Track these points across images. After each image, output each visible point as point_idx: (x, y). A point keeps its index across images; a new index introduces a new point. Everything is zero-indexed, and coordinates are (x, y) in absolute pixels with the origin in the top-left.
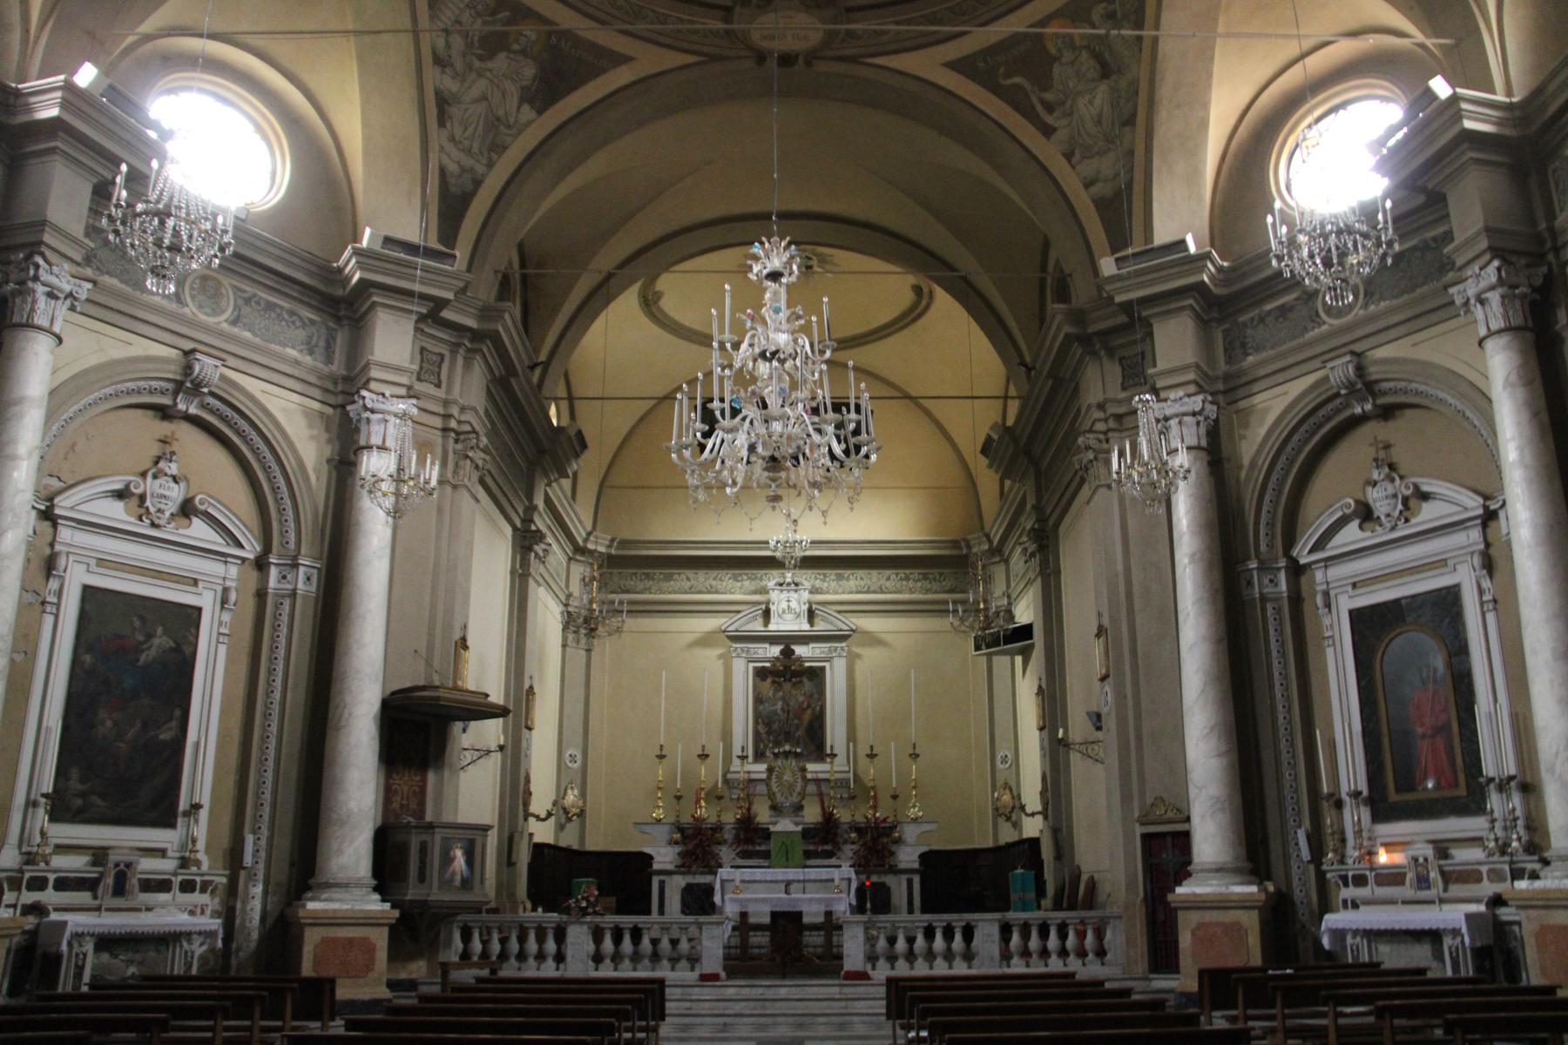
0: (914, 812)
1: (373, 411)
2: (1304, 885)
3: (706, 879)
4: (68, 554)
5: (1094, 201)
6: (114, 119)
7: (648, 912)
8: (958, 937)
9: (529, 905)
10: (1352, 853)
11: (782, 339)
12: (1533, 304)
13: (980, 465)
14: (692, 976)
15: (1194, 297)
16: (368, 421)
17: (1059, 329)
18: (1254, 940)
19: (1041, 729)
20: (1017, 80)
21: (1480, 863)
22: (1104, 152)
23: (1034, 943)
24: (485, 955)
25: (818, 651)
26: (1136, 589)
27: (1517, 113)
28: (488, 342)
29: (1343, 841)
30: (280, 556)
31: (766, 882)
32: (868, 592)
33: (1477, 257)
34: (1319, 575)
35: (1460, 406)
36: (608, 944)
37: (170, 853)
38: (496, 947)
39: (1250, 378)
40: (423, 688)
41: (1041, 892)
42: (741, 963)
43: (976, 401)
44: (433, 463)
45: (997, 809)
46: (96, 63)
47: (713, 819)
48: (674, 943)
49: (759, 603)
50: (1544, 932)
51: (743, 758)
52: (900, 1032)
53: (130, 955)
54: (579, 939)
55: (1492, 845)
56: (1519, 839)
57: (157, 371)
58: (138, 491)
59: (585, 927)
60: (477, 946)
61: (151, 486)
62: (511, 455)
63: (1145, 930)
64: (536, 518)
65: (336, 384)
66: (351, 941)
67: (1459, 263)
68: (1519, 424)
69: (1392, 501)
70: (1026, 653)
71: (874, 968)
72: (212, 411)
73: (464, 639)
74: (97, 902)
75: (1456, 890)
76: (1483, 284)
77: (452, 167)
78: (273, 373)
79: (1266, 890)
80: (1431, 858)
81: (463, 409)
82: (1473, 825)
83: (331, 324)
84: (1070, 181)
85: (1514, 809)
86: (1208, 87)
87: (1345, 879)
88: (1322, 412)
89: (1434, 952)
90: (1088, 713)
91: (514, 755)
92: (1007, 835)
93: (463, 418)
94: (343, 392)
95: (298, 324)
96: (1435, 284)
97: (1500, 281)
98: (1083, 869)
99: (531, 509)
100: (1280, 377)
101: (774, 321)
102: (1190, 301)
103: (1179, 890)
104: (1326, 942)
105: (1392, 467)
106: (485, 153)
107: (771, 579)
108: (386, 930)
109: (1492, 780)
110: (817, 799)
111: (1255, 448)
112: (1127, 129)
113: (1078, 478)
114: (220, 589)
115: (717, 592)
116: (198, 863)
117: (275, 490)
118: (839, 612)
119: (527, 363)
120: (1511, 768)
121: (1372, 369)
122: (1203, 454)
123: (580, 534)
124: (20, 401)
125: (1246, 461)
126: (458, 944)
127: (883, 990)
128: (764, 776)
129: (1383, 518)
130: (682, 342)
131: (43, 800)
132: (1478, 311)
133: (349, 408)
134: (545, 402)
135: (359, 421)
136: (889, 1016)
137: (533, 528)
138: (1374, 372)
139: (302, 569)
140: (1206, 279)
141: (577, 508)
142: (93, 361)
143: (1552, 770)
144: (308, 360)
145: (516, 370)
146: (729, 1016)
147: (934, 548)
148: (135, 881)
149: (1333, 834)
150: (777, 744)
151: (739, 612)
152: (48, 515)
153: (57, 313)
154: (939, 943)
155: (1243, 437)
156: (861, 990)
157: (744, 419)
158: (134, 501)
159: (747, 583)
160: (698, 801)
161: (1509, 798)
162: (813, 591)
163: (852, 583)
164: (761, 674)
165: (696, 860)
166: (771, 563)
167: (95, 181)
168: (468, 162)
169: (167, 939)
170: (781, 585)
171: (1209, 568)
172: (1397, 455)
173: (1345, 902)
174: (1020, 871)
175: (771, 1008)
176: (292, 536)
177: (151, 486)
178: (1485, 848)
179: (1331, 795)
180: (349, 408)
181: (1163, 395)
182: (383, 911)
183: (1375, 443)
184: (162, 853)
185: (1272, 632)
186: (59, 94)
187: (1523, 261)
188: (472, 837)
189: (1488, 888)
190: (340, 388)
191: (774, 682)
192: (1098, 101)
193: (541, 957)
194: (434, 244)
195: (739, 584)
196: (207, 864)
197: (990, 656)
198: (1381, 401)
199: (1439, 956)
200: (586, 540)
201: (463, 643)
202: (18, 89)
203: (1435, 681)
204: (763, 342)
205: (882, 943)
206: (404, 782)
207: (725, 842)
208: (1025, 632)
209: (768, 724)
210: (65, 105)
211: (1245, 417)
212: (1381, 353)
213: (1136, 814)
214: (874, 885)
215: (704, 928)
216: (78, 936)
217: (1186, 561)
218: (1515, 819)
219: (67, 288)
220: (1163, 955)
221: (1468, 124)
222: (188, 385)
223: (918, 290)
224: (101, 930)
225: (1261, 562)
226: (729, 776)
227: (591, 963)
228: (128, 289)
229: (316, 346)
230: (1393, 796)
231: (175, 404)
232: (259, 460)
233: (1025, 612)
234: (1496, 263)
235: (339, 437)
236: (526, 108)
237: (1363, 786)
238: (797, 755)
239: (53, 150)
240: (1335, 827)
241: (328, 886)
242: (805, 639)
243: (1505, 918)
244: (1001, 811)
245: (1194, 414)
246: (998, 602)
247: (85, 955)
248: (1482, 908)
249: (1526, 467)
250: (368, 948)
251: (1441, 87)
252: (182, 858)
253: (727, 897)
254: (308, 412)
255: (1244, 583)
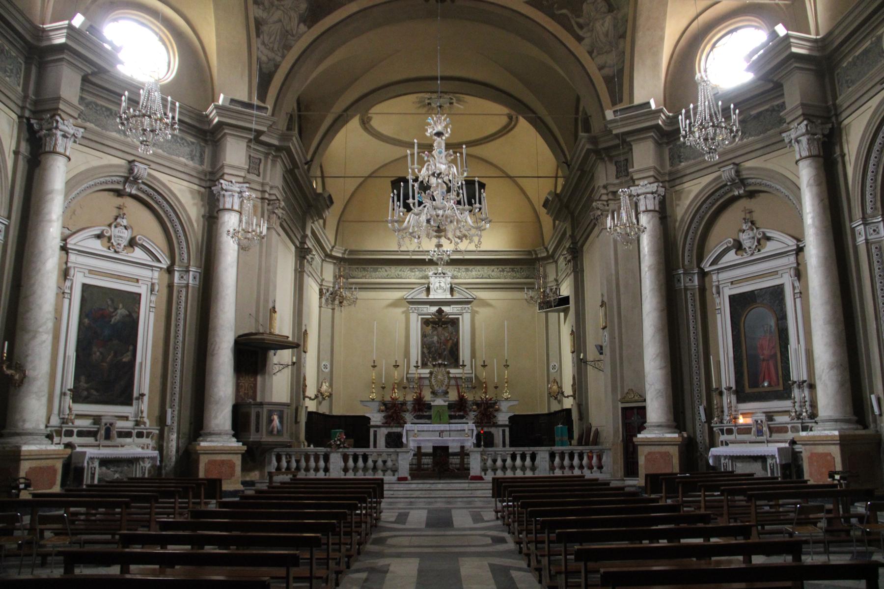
0: (506, 395)
1: (226, 191)
2: (702, 434)
3: (399, 430)
4: (74, 267)
5: (603, 78)
6: (93, 42)
7: (368, 446)
8: (528, 459)
9: (306, 444)
10: (726, 418)
11: (443, 167)
12: (824, 143)
13: (543, 211)
14: (394, 478)
15: (654, 132)
16: (224, 196)
17: (584, 146)
18: (676, 461)
19: (573, 352)
20: (564, 11)
21: (788, 423)
22: (609, 52)
23: (566, 462)
24: (288, 468)
25: (455, 309)
26: (621, 282)
27: (820, 44)
28: (284, 152)
29: (723, 412)
30: (180, 266)
31: (429, 431)
32: (482, 278)
33: (796, 118)
34: (714, 277)
35: (787, 193)
36: (351, 463)
37: (130, 418)
38: (294, 465)
39: (682, 174)
40: (256, 334)
41: (571, 437)
42: (418, 472)
43: (540, 179)
44: (264, 222)
45: (550, 393)
46: (84, 14)
47: (401, 399)
48: (385, 462)
49: (424, 284)
50: (812, 455)
51: (417, 367)
52: (498, 503)
53: (115, 469)
54: (336, 460)
55: (793, 414)
56: (806, 412)
57: (115, 172)
58: (107, 235)
59: (339, 454)
60: (284, 464)
61: (114, 232)
62: (294, 209)
63: (622, 456)
64: (307, 242)
65: (205, 175)
66: (223, 462)
67: (788, 121)
68: (813, 205)
69: (752, 240)
70: (566, 311)
71: (485, 474)
72: (144, 192)
73: (274, 308)
74: (97, 443)
75: (776, 436)
76: (799, 133)
77: (264, 59)
78: (172, 170)
79: (683, 436)
80: (764, 420)
81: (271, 188)
82: (786, 404)
83: (203, 144)
84: (592, 67)
85: (805, 397)
86: (664, 19)
87: (722, 431)
88: (717, 194)
89: (762, 468)
90: (596, 346)
91: (297, 366)
92: (555, 407)
93: (272, 192)
94: (210, 180)
95: (185, 144)
96: (778, 130)
97: (807, 132)
98: (593, 425)
99: (305, 236)
100: (697, 175)
101: (439, 157)
102: (652, 134)
103: (639, 436)
104: (711, 462)
105: (753, 223)
106: (281, 50)
107: (430, 271)
108: (240, 456)
109: (796, 382)
110: (455, 387)
111: (684, 211)
112: (621, 41)
113: (592, 224)
114: (150, 284)
115: (401, 278)
116: (144, 423)
117: (176, 232)
118: (467, 289)
119: (304, 161)
120: (805, 377)
121: (744, 172)
122: (657, 214)
123: (328, 248)
124: (51, 192)
125: (679, 218)
126: (274, 462)
127: (490, 485)
128: (428, 376)
129: (747, 249)
130: (382, 143)
131: (69, 392)
132: (796, 147)
133: (213, 188)
134: (311, 179)
135: (219, 195)
136: (493, 497)
137: (306, 247)
138: (745, 174)
139: (191, 273)
140: (660, 122)
141: (326, 232)
142: (83, 168)
143: (820, 379)
144: (191, 163)
145: (297, 164)
146: (413, 498)
147: (516, 255)
148: (115, 432)
149: (717, 408)
150: (434, 359)
151: (413, 288)
152: (64, 249)
153: (68, 145)
154: (518, 462)
155: (677, 205)
156: (479, 485)
157: (425, 207)
158: (106, 240)
159: (417, 273)
160: (394, 389)
161: (803, 391)
162: (453, 277)
163: (474, 273)
164: (426, 322)
165: (393, 419)
166: (431, 262)
167: (83, 74)
168: (271, 55)
169: (132, 461)
170: (436, 274)
171: (658, 273)
172: (756, 216)
173: (722, 442)
174: (560, 426)
175: (433, 494)
176: (185, 256)
177: (114, 232)
178: (790, 416)
179: (717, 389)
180: (213, 188)
181: (637, 182)
182: (238, 447)
183: (745, 210)
184: (126, 418)
185: (690, 306)
186: (65, 31)
187: (819, 121)
188: (280, 408)
189: (790, 436)
190: (208, 177)
191: (433, 327)
192: (606, 24)
193: (317, 469)
194: (255, 101)
195: (413, 274)
196: (149, 425)
197: (547, 313)
198: (748, 189)
199: (765, 469)
200: (331, 251)
201: (274, 310)
202: (43, 28)
203: (771, 332)
204: (433, 167)
205: (489, 462)
206: (246, 381)
207: (408, 410)
208: (565, 301)
209: (429, 348)
210: (68, 36)
211: (679, 194)
212: (748, 164)
213: (619, 397)
214: (485, 433)
215: (400, 454)
216: (92, 459)
217: (647, 269)
218: (805, 402)
219: (72, 132)
220: (631, 469)
221: (794, 50)
222: (132, 179)
223: (510, 118)
224: (102, 456)
225: (685, 270)
226: (408, 376)
227: (342, 472)
228: (99, 129)
229: (195, 155)
230: (748, 390)
231: (125, 189)
232: (167, 217)
233: (566, 290)
234: (805, 122)
235: (208, 203)
236: (302, 26)
237: (733, 385)
238: (445, 365)
239: (62, 60)
240: (719, 405)
241: (210, 434)
242: (448, 303)
243: (797, 450)
244: (552, 394)
245: (652, 193)
246: (552, 284)
247: (95, 468)
248: (787, 445)
249: (816, 227)
250: (232, 465)
251: (781, 30)
252: (136, 421)
253: (411, 438)
254: (192, 191)
255: (676, 280)
